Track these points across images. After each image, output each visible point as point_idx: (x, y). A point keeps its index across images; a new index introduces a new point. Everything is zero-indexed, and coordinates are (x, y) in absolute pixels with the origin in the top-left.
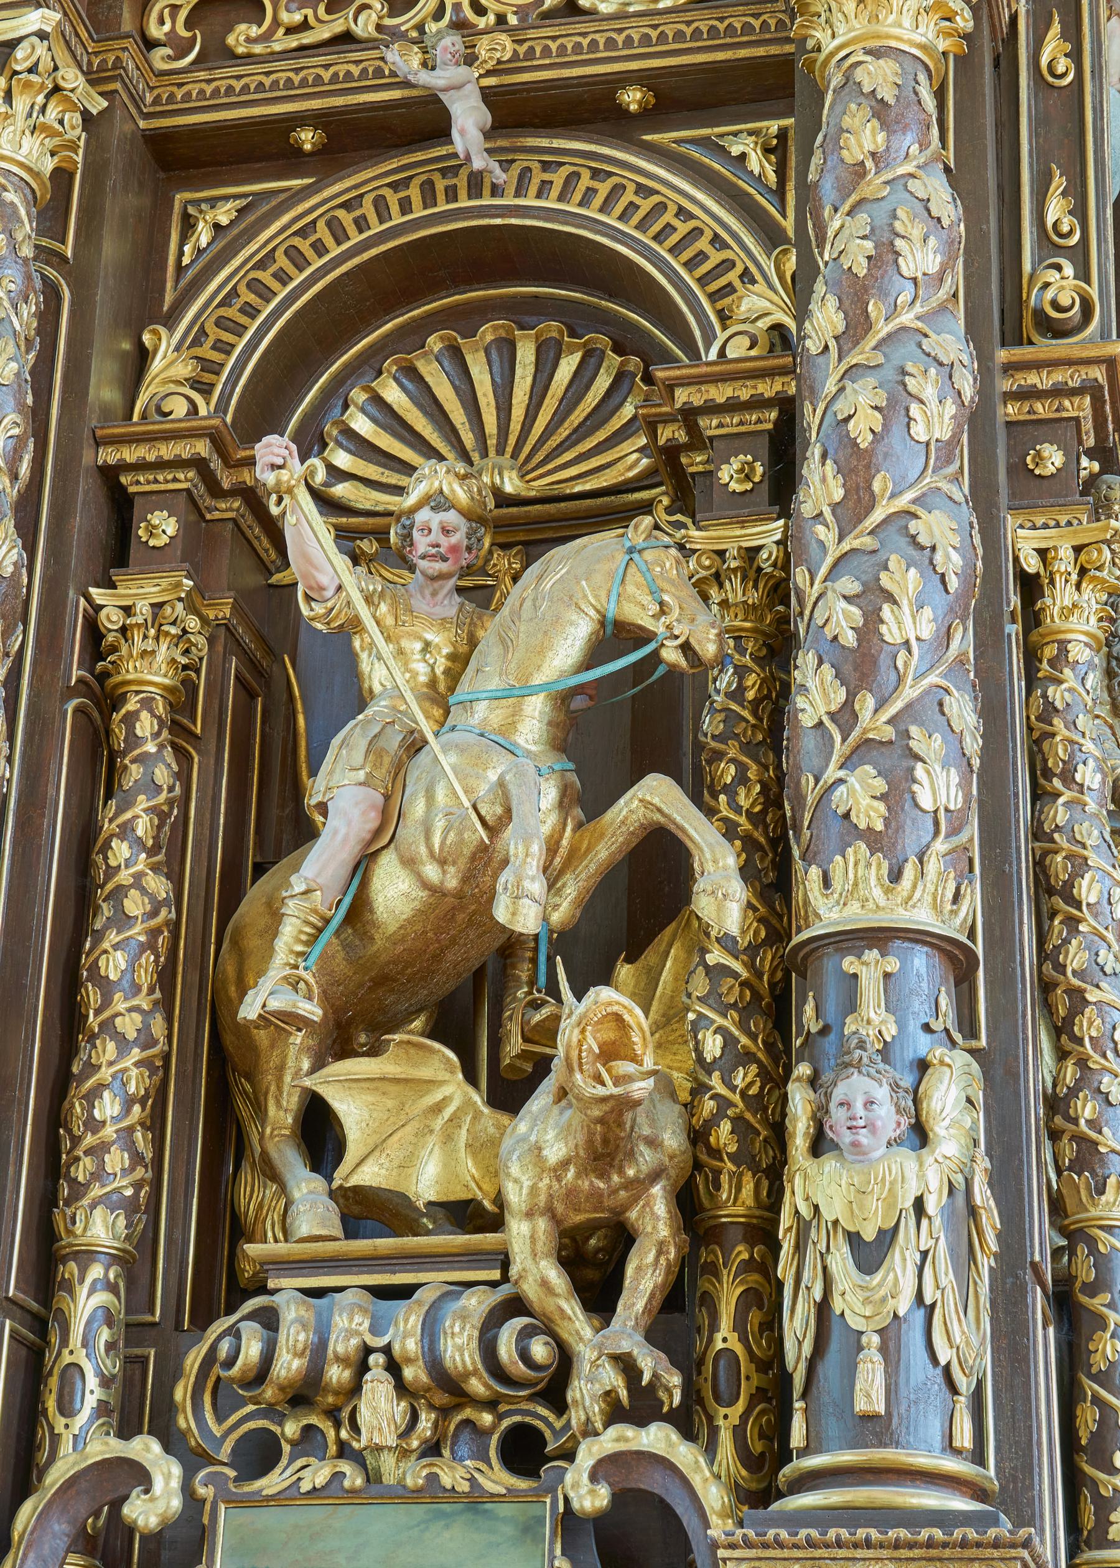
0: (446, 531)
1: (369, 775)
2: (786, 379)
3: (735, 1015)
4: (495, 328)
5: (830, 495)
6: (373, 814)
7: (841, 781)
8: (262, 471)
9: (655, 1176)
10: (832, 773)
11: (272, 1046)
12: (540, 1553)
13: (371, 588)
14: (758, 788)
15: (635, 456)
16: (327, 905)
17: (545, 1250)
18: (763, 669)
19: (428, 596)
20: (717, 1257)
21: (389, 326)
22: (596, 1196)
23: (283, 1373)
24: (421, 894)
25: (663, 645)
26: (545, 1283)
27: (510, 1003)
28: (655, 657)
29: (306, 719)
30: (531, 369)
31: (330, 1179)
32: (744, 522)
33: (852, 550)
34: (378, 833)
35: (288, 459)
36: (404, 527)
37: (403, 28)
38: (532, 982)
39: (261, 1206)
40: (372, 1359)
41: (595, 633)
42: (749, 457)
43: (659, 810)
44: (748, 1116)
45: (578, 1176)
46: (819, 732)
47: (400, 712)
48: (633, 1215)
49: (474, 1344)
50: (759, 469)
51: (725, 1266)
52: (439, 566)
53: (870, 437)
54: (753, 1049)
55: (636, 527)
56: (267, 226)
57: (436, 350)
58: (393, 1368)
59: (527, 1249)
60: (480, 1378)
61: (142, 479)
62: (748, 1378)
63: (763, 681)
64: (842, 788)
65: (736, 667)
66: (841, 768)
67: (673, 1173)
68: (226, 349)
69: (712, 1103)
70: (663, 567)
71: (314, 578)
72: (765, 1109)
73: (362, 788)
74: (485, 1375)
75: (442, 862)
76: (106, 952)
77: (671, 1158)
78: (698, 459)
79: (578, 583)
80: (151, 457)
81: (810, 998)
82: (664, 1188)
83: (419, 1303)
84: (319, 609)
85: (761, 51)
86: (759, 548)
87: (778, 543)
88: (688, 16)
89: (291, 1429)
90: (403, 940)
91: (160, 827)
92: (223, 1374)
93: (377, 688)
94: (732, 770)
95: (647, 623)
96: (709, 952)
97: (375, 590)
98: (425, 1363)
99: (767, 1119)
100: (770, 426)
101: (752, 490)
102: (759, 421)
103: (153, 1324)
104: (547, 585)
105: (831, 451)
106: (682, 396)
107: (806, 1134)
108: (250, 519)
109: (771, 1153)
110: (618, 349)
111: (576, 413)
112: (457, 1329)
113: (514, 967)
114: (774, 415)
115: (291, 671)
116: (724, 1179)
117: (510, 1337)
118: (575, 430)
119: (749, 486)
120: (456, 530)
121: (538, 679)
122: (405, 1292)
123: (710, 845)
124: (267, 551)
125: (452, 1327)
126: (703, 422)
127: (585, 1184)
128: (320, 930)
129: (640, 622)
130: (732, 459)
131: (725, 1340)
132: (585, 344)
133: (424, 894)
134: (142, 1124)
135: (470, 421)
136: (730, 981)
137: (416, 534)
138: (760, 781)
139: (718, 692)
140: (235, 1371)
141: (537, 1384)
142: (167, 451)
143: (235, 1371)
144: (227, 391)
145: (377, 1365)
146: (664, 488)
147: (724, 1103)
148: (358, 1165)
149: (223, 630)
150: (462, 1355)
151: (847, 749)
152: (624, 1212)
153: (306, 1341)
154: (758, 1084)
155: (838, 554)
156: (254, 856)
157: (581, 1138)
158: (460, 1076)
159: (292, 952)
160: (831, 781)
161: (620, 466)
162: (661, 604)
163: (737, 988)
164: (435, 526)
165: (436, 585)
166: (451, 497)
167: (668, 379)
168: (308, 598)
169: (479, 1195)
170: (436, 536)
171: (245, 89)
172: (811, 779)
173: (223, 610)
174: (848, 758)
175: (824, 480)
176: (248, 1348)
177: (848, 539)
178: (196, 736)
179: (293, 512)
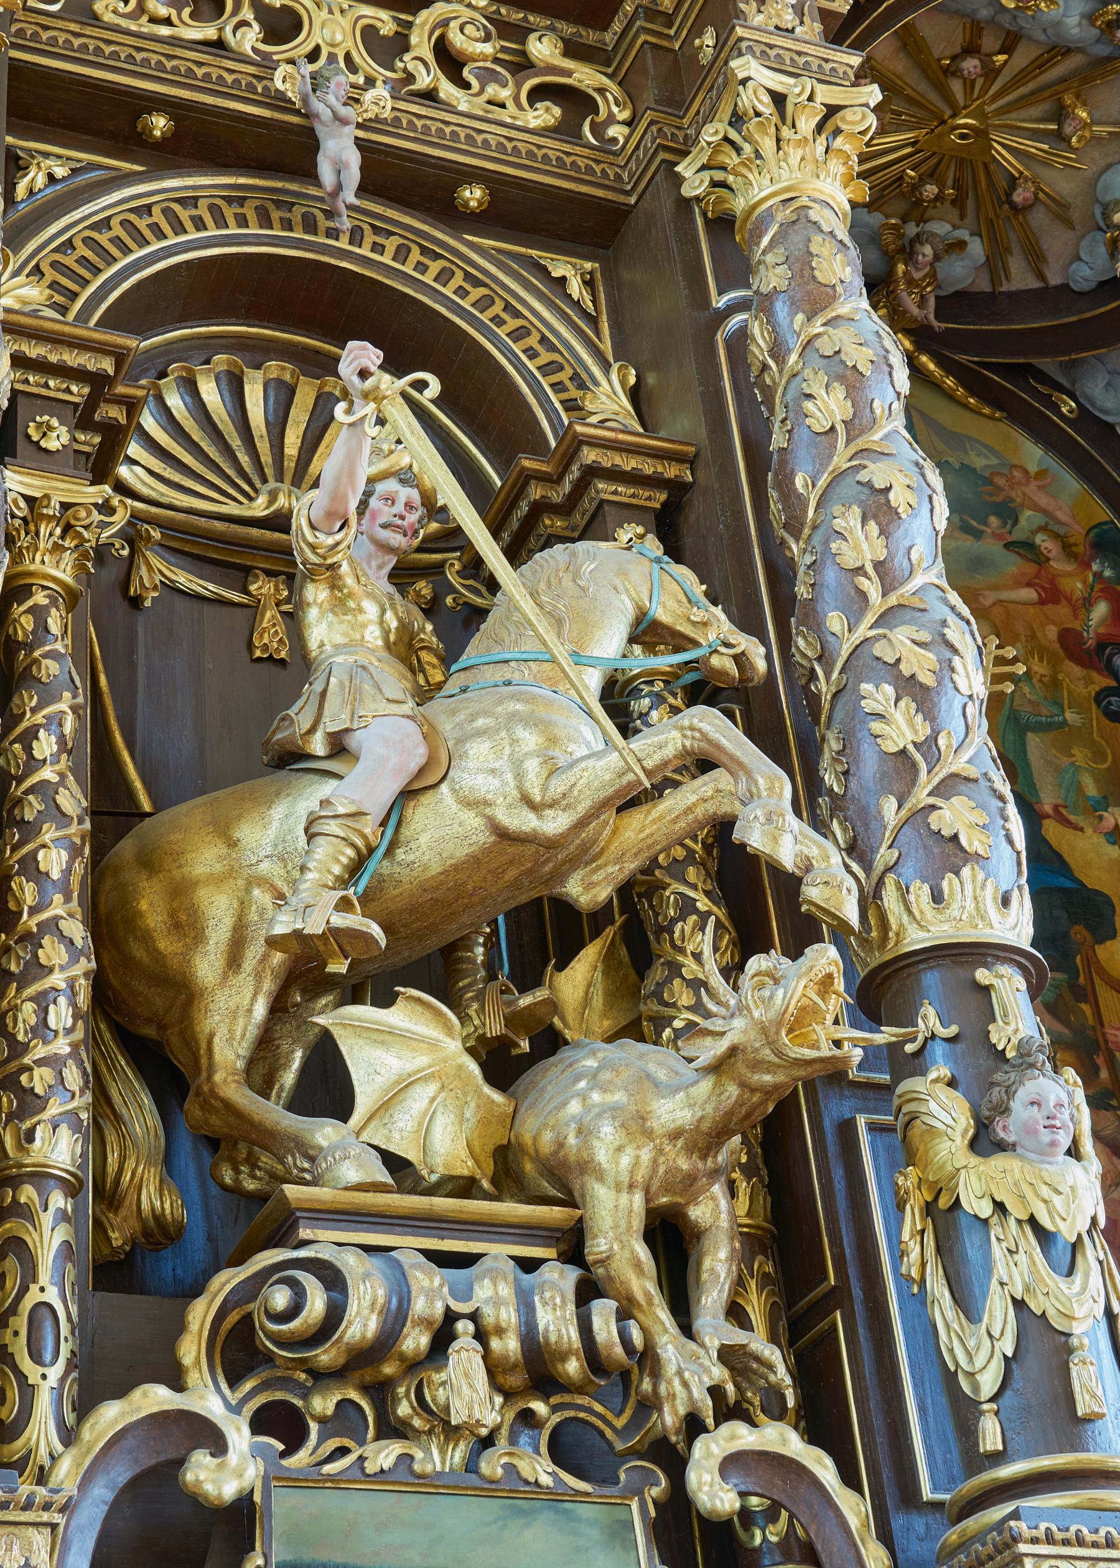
12: (633, 1561)
34: (421, 772)
37: (275, 57)
46: (900, 759)
56: (108, 192)
58: (481, 1336)
61: (31, 379)
76: (44, 846)
80: (53, 358)
85: (600, 193)
88: (541, 141)
89: (324, 1404)
100: (658, 506)
102: (649, 499)
106: (589, 455)
114: (663, 497)
133: (492, 839)
142: (72, 359)
148: (369, 1119)
167: (582, 435)
170: (399, 508)
171: (115, 55)
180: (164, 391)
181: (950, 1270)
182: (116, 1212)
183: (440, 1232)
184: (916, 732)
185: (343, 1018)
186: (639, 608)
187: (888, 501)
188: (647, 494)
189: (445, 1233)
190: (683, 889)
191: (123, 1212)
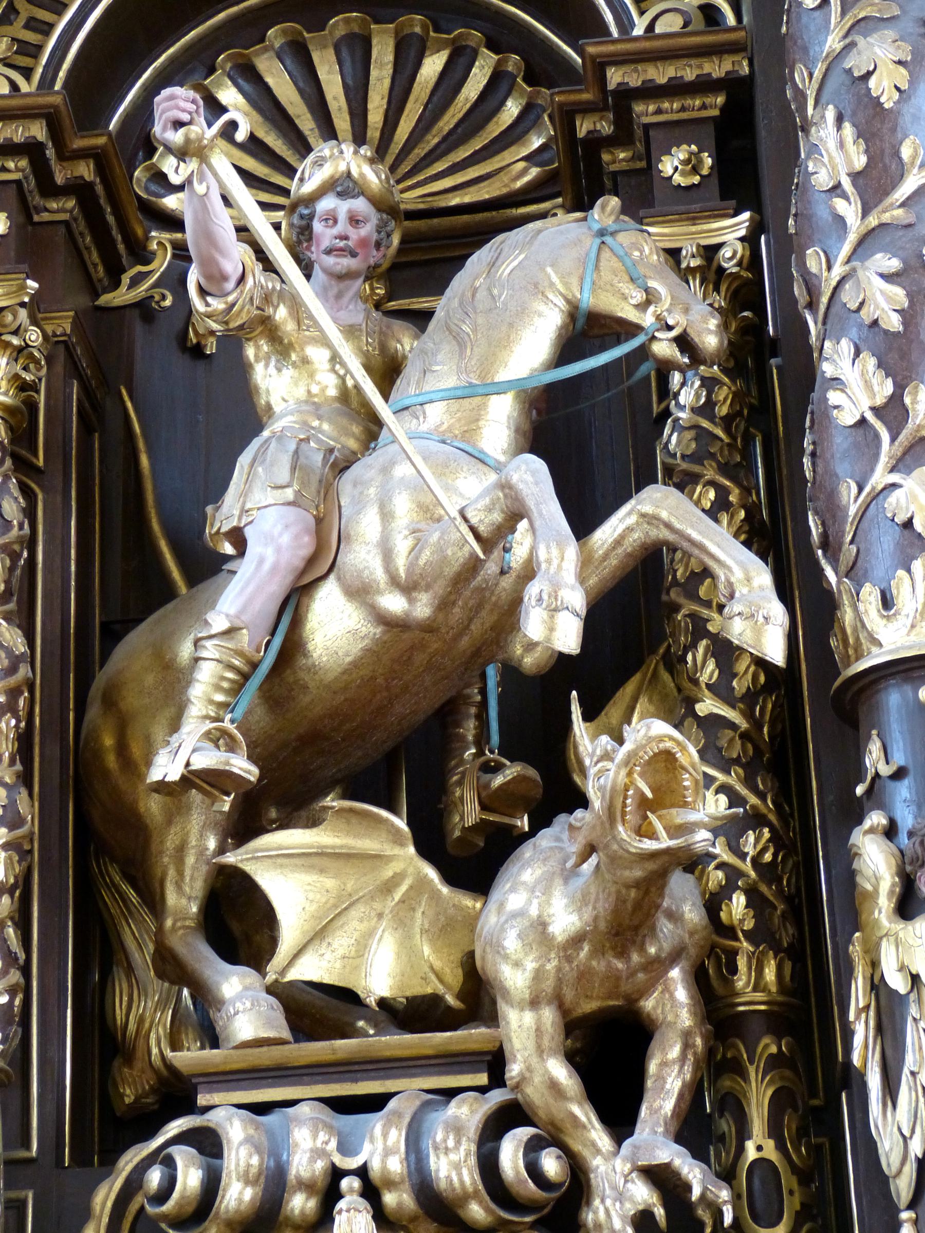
0: (354, 220)
1: (298, 493)
2: (737, 58)
3: (740, 771)
4: (347, 21)
5: (849, 161)
6: (306, 539)
7: (894, 486)
8: (164, 129)
9: (674, 958)
10: (880, 477)
11: (169, 822)
13: (270, 285)
14: (742, 514)
15: (522, 165)
16: (254, 646)
17: (553, 1045)
18: (733, 380)
19: (332, 299)
20: (739, 1051)
21: (222, 16)
22: (614, 978)
23: (233, 1204)
24: (372, 630)
25: (653, 338)
26: (554, 1086)
27: (457, 766)
28: (643, 353)
29: (150, 458)
30: (388, 70)
31: (263, 974)
32: (694, 218)
33: (882, 225)
34: (311, 561)
35: (195, 115)
36: (302, 217)
38: (482, 740)
39: (141, 1020)
40: (345, 1183)
41: (564, 327)
42: (694, 147)
43: (668, 526)
44: (764, 888)
45: (594, 953)
46: (860, 431)
47: (313, 428)
48: (649, 1004)
49: (473, 1161)
50: (709, 162)
51: (751, 1063)
52: (346, 263)
53: (896, 96)
54: (764, 810)
55: (603, 208)
57: (277, 45)
59: (531, 1044)
60: (481, 1203)
62: (791, 1193)
63: (735, 395)
64: (898, 493)
65: (703, 379)
66: (891, 471)
67: (693, 951)
68: (46, 29)
69: (720, 874)
70: (642, 252)
71: (217, 264)
72: (781, 879)
73: (292, 509)
74: (487, 1198)
75: (408, 588)
77: (691, 934)
78: (622, 155)
79: (543, 270)
81: (875, 737)
82: (683, 970)
83: (398, 1114)
84: (217, 305)
86: (720, 246)
87: (742, 239)
90: (345, 688)
91: (11, 569)
92: (150, 1209)
93: (278, 407)
94: (712, 494)
95: (631, 315)
96: (698, 701)
97: (274, 288)
98: (412, 1186)
99: (782, 891)
100: (716, 112)
101: (700, 184)
102: (704, 107)
103: (31, 1161)
104: (505, 270)
105: (847, 113)
106: (615, 77)
107: (891, 892)
108: (81, 226)
109: (791, 931)
110: (493, 46)
111: (446, 117)
112: (451, 1143)
113: (458, 725)
114: (720, 100)
115: (129, 405)
116: (742, 962)
117: (516, 1151)
118: (445, 138)
119: (696, 179)
120: (366, 220)
121: (503, 376)
122: (375, 1103)
123: (740, 564)
124: (95, 265)
125: (445, 1141)
126: (638, 108)
127: (599, 965)
128: (246, 677)
129: (620, 314)
130: (674, 150)
131: (759, 1148)
132: (454, 41)
133: (379, 630)
134: (12, 919)
135: (319, 127)
136: (729, 733)
137: (317, 226)
138: (744, 507)
139: (682, 408)
140: (169, 1206)
141: (544, 1207)
143: (169, 1206)
144: (50, 76)
145: (351, 1190)
146: (560, 200)
147: (733, 873)
149: (61, 348)
150: (460, 1175)
151: (898, 449)
152: (637, 1000)
153: (261, 1165)
154: (772, 850)
155: (863, 230)
156: (100, 615)
157: (604, 906)
158: (411, 850)
159: (211, 702)
160: (880, 487)
161: (504, 177)
162: (647, 290)
163: (738, 742)
164: (342, 216)
165: (342, 285)
166: (361, 182)
168: (203, 292)
169: (441, 989)
170: (342, 226)
172: (854, 489)
173: (63, 324)
174: (900, 460)
175: (841, 145)
176: (185, 1177)
177: (875, 212)
178: (38, 470)
179: (201, 182)
180: (214, 90)
181: (889, 1053)
182: (131, 1066)
183: (352, 1075)
184: (873, 395)
185: (257, 851)
186: (568, 301)
187: (869, 90)
188: (698, 102)
189: (359, 1075)
190: (695, 607)
191: (138, 1065)
